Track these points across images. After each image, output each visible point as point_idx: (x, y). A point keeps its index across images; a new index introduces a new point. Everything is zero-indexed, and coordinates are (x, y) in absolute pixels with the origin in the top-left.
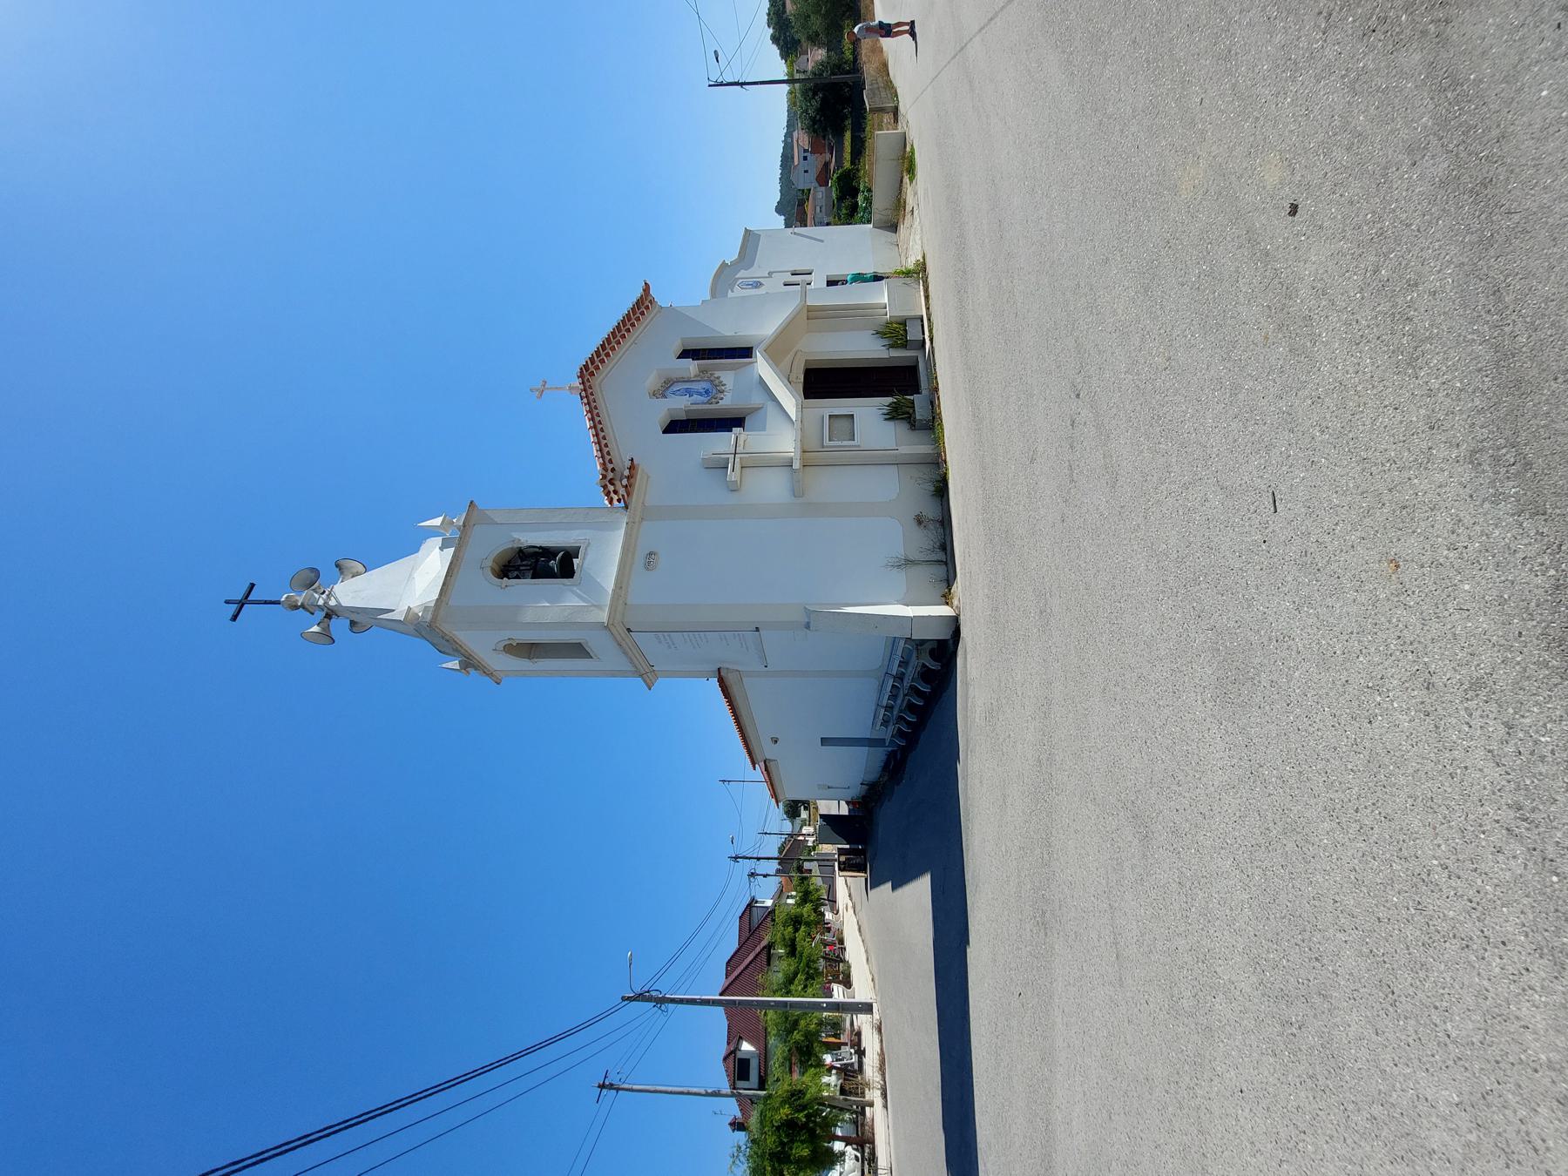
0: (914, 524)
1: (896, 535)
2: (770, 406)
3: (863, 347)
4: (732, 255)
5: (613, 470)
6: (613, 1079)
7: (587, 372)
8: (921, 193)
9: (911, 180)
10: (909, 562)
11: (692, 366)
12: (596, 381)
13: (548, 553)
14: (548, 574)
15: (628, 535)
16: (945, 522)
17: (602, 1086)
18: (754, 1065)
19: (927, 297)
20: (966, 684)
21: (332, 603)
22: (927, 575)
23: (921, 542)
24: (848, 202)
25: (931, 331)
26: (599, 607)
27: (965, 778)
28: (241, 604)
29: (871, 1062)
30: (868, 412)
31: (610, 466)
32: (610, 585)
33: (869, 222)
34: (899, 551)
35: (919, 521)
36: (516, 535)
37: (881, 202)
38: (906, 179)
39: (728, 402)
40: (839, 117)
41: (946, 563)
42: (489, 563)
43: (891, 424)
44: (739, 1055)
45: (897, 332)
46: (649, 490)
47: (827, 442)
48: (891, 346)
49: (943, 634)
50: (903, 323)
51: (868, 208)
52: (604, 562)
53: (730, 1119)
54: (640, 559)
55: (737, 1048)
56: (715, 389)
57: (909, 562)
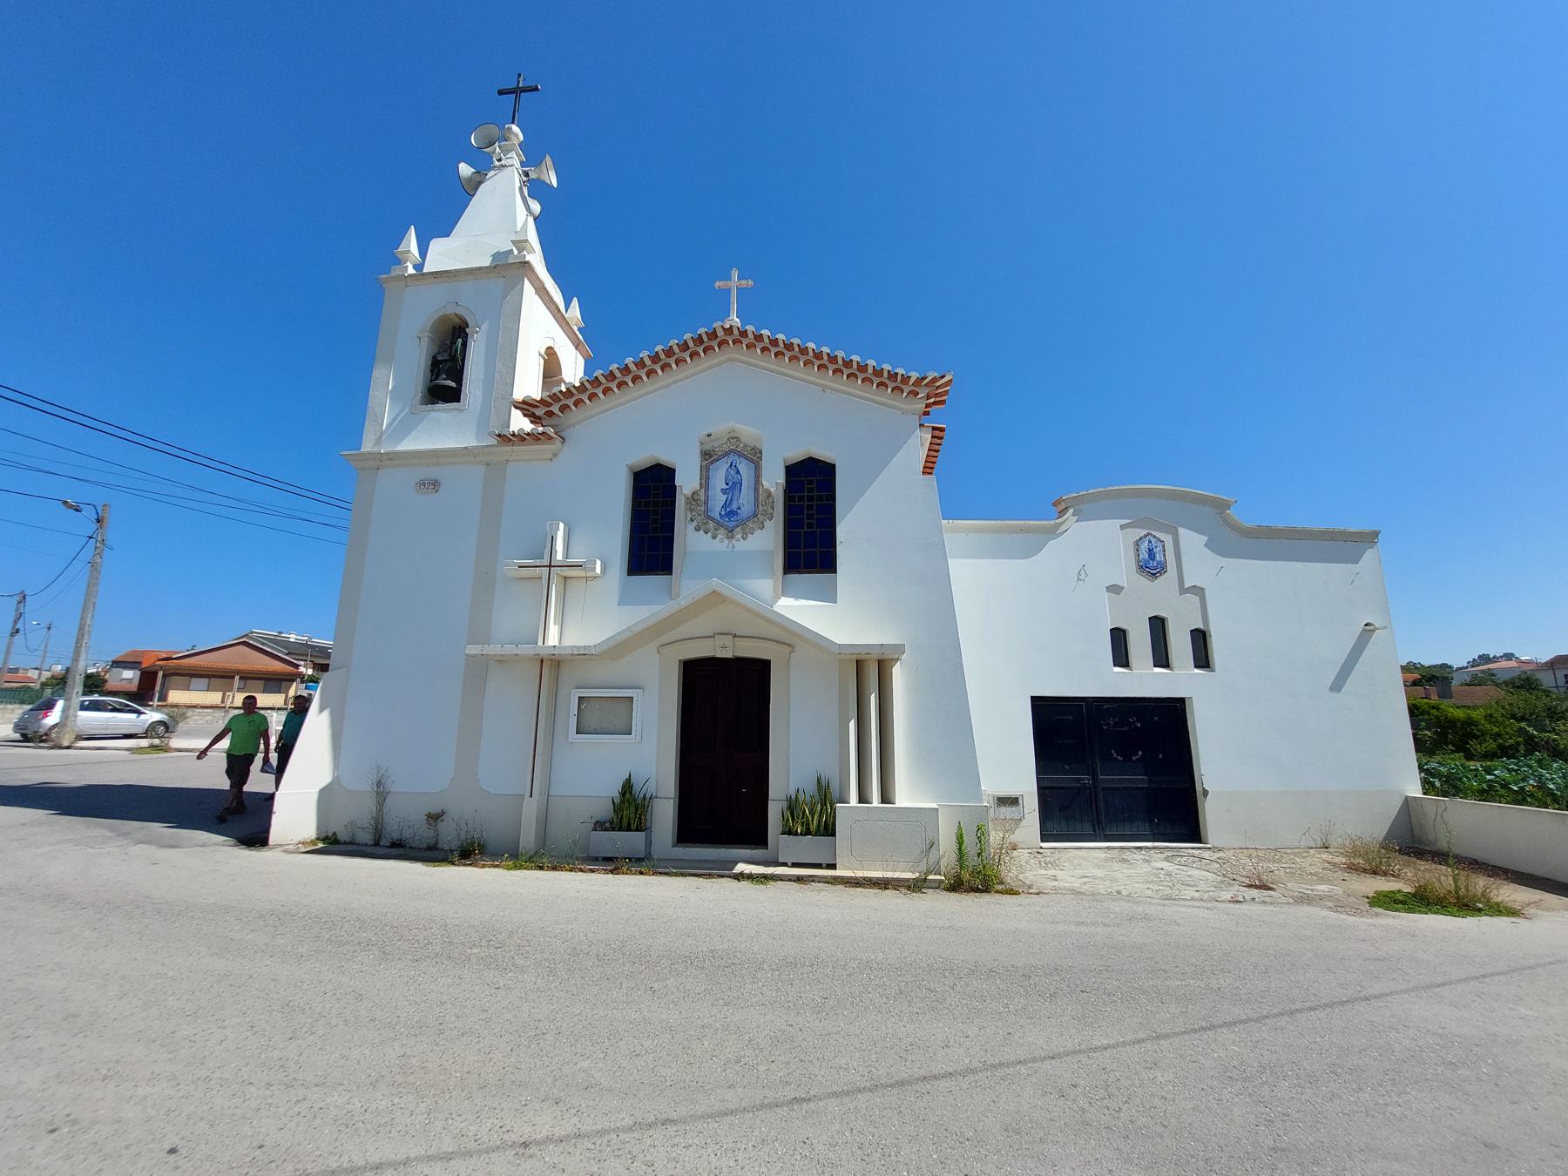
0: (435, 810)
1: (424, 783)
3: (799, 748)
5: (550, 414)
10: (381, 794)
11: (774, 480)
13: (458, 374)
14: (436, 366)
16: (432, 853)
19: (883, 884)
22: (356, 815)
23: (405, 816)
26: (378, 441)
27: (423, 366)
30: (650, 753)
32: (406, 446)
33: (1427, 787)
34: (397, 786)
35: (435, 818)
37: (1471, 821)
39: (690, 540)
41: (377, 844)
42: (450, 310)
43: (614, 790)
45: (817, 818)
48: (792, 806)
50: (829, 830)
52: (444, 431)
54: (430, 474)
56: (731, 521)
57: (381, 794)
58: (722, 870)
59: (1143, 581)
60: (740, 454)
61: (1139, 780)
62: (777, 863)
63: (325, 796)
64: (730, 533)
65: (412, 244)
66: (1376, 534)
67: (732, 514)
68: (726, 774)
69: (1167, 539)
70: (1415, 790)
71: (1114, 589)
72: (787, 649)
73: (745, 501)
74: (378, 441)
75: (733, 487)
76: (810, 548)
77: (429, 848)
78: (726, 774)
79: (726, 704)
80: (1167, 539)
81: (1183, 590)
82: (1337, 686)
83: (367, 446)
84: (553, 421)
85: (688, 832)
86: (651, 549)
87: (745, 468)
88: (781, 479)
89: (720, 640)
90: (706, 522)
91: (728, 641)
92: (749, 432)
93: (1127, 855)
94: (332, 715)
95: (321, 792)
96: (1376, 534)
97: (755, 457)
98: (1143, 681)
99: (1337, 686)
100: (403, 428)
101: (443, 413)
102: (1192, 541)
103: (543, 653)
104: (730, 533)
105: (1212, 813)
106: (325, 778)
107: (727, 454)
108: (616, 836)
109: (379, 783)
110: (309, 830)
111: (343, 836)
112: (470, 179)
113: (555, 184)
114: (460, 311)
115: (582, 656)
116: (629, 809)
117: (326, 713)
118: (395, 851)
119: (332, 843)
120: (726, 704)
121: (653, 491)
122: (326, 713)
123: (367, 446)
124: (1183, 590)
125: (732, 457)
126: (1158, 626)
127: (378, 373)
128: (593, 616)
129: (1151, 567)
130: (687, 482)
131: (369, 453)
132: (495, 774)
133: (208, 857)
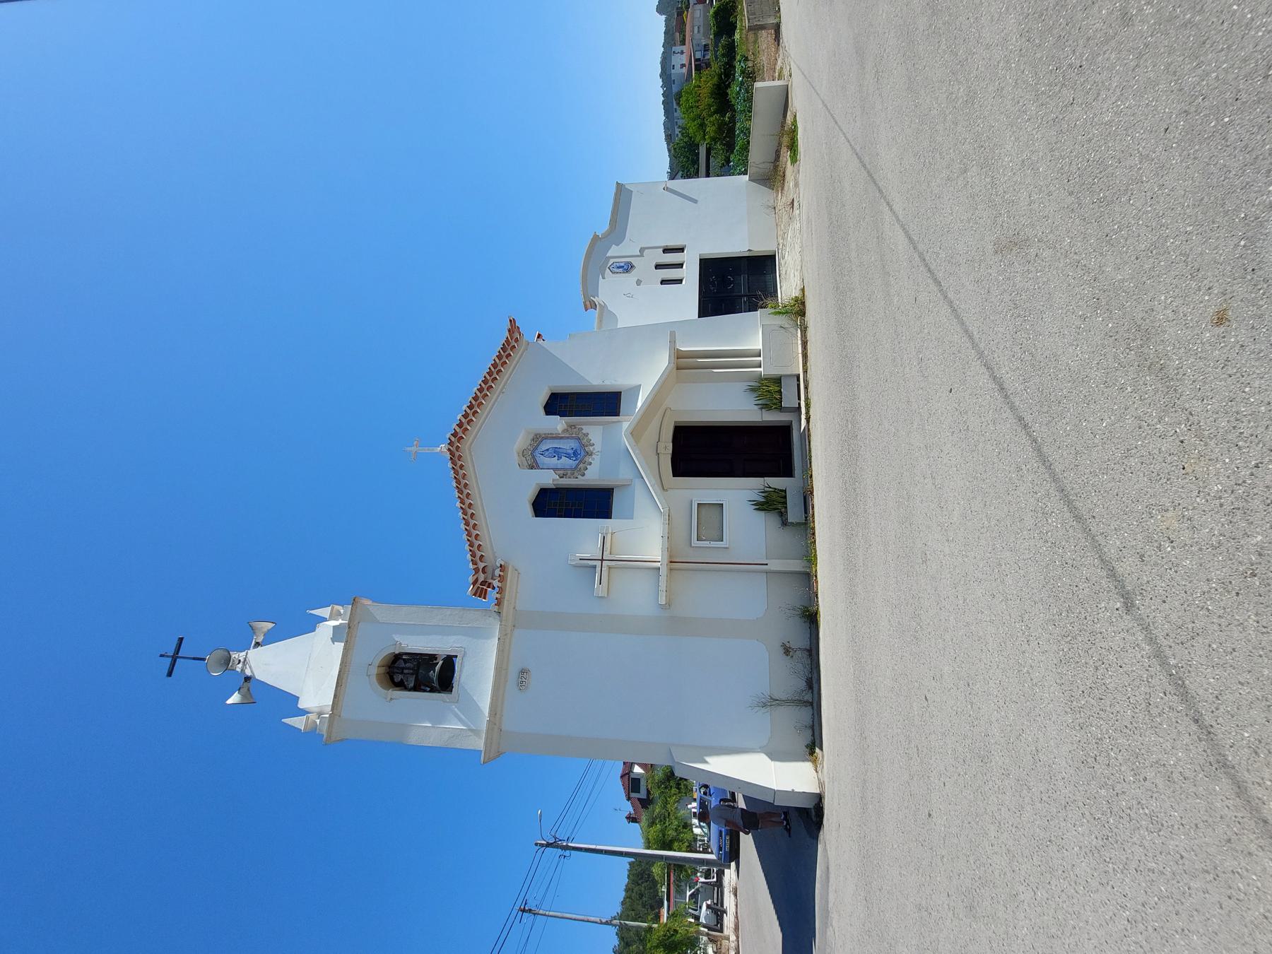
1: (761, 666)
2: (637, 483)
3: (732, 406)
4: (603, 227)
5: (484, 570)
6: (531, 905)
7: (457, 438)
8: (801, 177)
9: (794, 160)
10: (772, 702)
11: (558, 424)
12: (465, 446)
15: (501, 651)
17: (524, 911)
18: (643, 783)
20: (826, 912)
21: (248, 672)
24: (723, 41)
25: (807, 399)
26: (476, 732)
28: (174, 659)
29: (729, 921)
30: (735, 494)
31: (481, 565)
32: (485, 704)
33: (745, 173)
35: (787, 651)
36: (397, 638)
37: (758, 153)
38: (786, 155)
39: (593, 476)
40: (717, 120)
41: (811, 704)
42: (374, 671)
43: (762, 514)
44: (632, 776)
45: (770, 390)
46: (524, 591)
47: (695, 542)
48: (765, 407)
49: (808, 804)
50: (778, 381)
51: (745, 162)
52: (479, 677)
53: (627, 814)
54: (513, 677)
55: (631, 771)
56: (581, 454)
57: (772, 702)
58: (806, 436)
59: (634, 272)
60: (536, 448)
61: (743, 279)
62: (799, 407)
63: (774, 756)
64: (589, 454)
65: (298, 722)
66: (620, 187)
67: (575, 453)
68: (749, 450)
69: (612, 261)
70: (746, 177)
71: (639, 282)
72: (668, 412)
73: (568, 445)
74: (476, 732)
75: (557, 453)
76: (606, 403)
77: (810, 655)
78: (749, 450)
79: (701, 450)
80: (612, 261)
81: (642, 255)
82: (695, 201)
83: (479, 744)
84: (489, 570)
85: (786, 470)
86: (594, 503)
87: (544, 447)
88: (556, 418)
89: (661, 450)
90: (579, 470)
91: (661, 445)
92: (521, 441)
93: (783, 272)
94: (710, 755)
95: (772, 759)
96: (620, 187)
97: (538, 439)
98: (691, 274)
99: (695, 201)
100: (471, 708)
101: (462, 675)
102: (614, 251)
103: (666, 562)
104: (589, 454)
105: (760, 247)
106: (763, 758)
107: (533, 457)
108: (790, 513)
109: (764, 705)
110: (807, 766)
111: (808, 740)
112: (244, 696)
113: (230, 701)
114: (377, 662)
115: (669, 538)
116: (772, 504)
117: (708, 759)
118: (815, 686)
119: (812, 746)
120: (701, 450)
121: (550, 503)
122: (708, 759)
123: (479, 744)
124: (642, 255)
125: (537, 454)
126: (658, 267)
127: (414, 739)
128: (645, 529)
129: (628, 268)
130: (548, 479)
131: (486, 744)
132: (754, 604)
133: (836, 848)
